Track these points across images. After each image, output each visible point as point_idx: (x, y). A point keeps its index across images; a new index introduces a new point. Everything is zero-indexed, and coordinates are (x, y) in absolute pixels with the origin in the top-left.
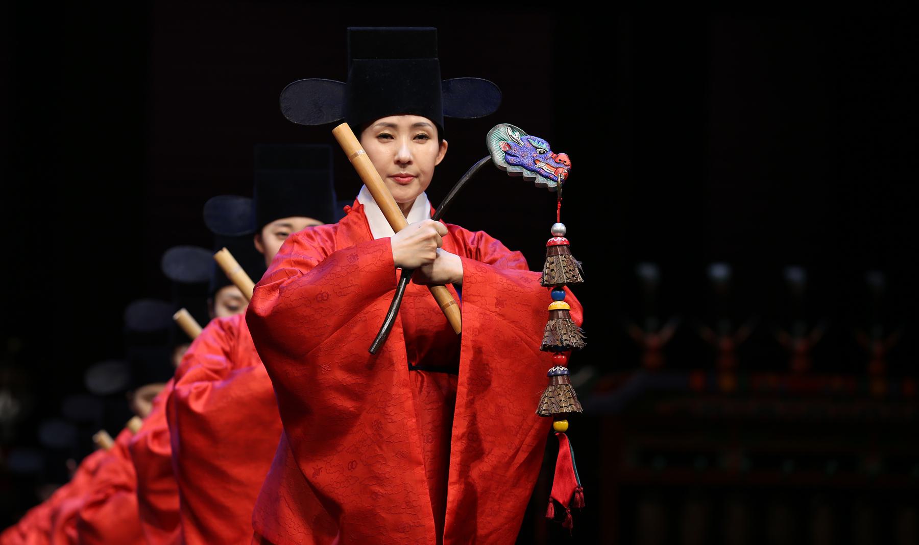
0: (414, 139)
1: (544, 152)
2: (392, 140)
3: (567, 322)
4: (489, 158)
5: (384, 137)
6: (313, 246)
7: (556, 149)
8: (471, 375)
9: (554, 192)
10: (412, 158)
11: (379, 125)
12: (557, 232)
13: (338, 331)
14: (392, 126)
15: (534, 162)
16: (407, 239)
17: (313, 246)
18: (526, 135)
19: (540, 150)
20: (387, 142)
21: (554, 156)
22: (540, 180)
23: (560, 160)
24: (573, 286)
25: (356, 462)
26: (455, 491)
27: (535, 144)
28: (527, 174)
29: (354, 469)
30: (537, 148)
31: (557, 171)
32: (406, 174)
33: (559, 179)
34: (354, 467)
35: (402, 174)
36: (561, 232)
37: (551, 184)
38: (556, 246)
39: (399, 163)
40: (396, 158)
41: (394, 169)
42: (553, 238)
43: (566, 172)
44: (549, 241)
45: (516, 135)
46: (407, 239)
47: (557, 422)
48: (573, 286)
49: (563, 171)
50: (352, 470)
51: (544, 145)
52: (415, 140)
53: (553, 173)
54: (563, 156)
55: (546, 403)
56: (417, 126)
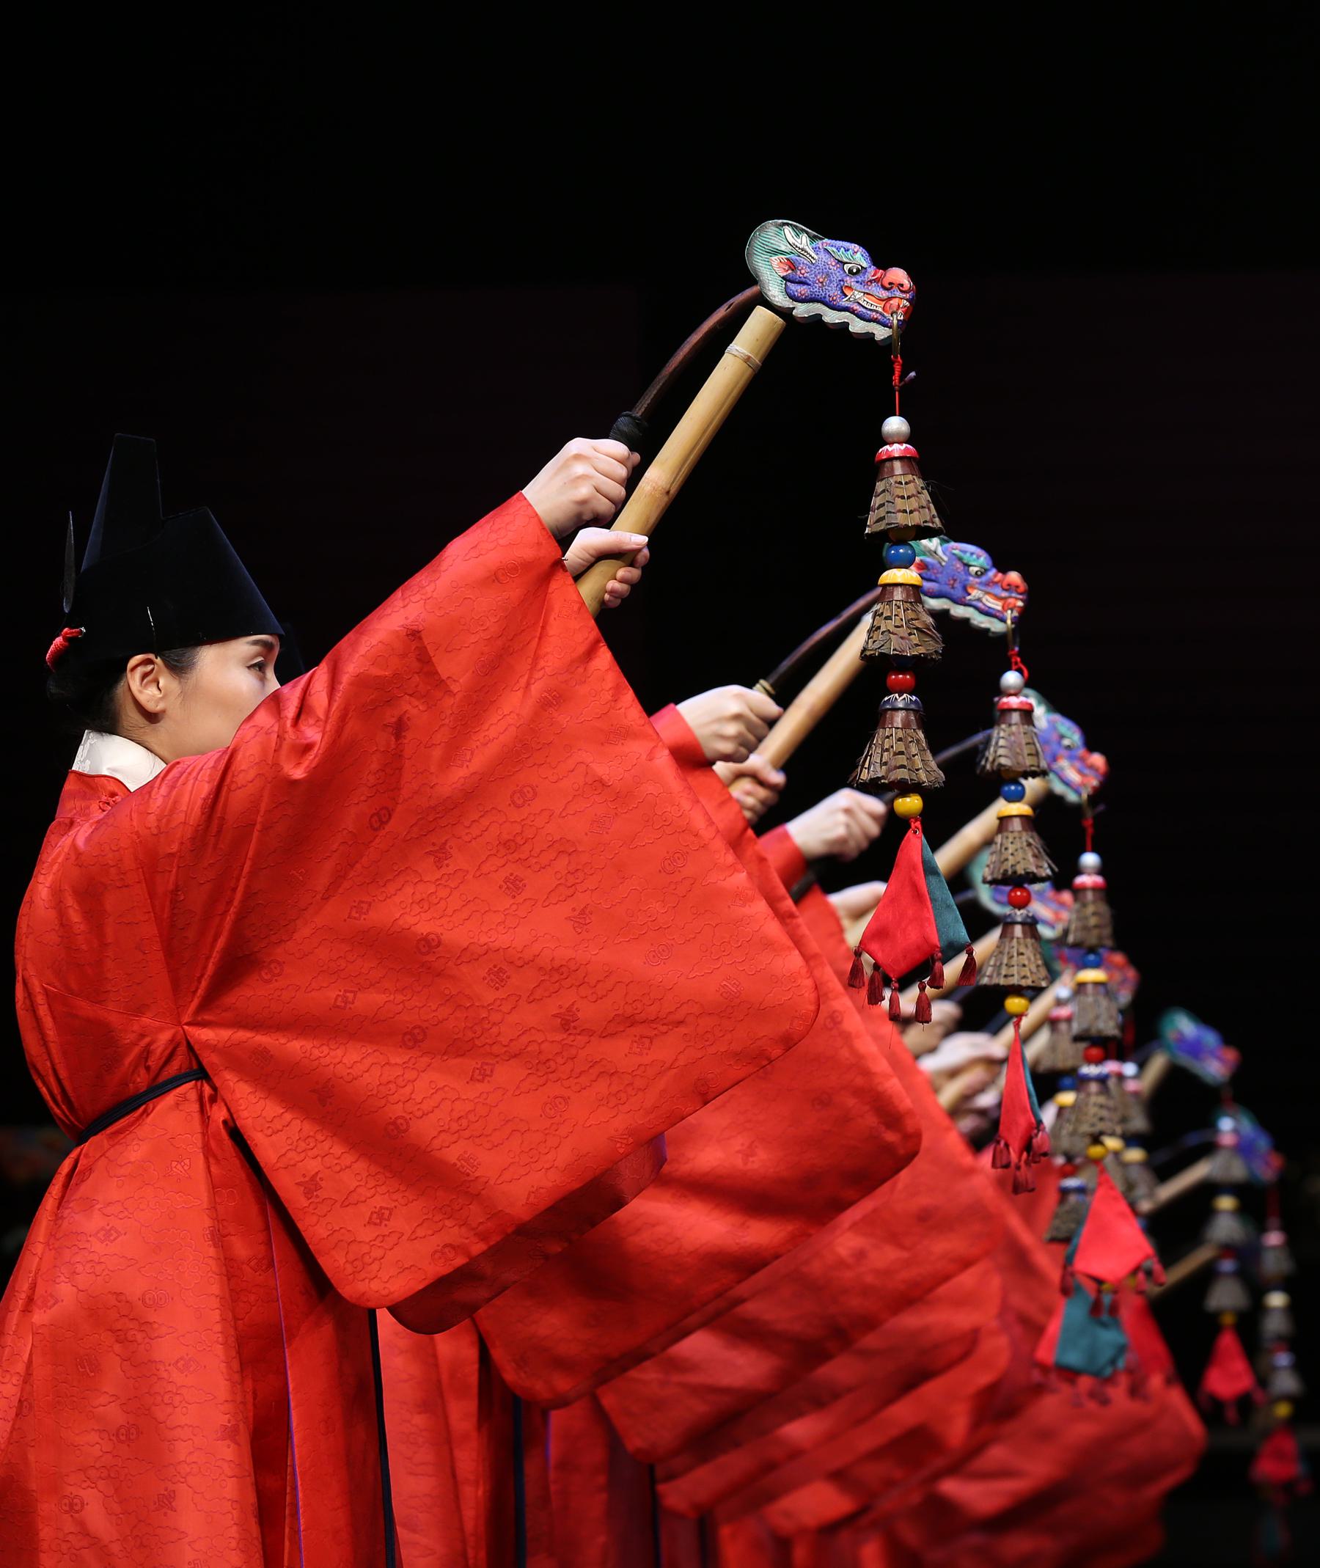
1: (858, 271)
4: (754, 289)
7: (882, 261)
8: (1007, 770)
9: (887, 345)
12: (891, 435)
13: (286, 1346)
15: (843, 292)
16: (33, 1287)
18: (821, 239)
19: (850, 265)
21: (879, 275)
22: (857, 326)
23: (890, 284)
27: (842, 255)
28: (831, 317)
31: (888, 305)
33: (895, 322)
36: (898, 434)
37: (881, 333)
38: (892, 459)
42: (887, 447)
43: (908, 304)
44: (880, 450)
45: (803, 241)
46: (33, 1287)
47: (900, 800)
49: (901, 302)
51: (857, 256)
53: (880, 310)
54: (899, 275)
55: (374, 753)
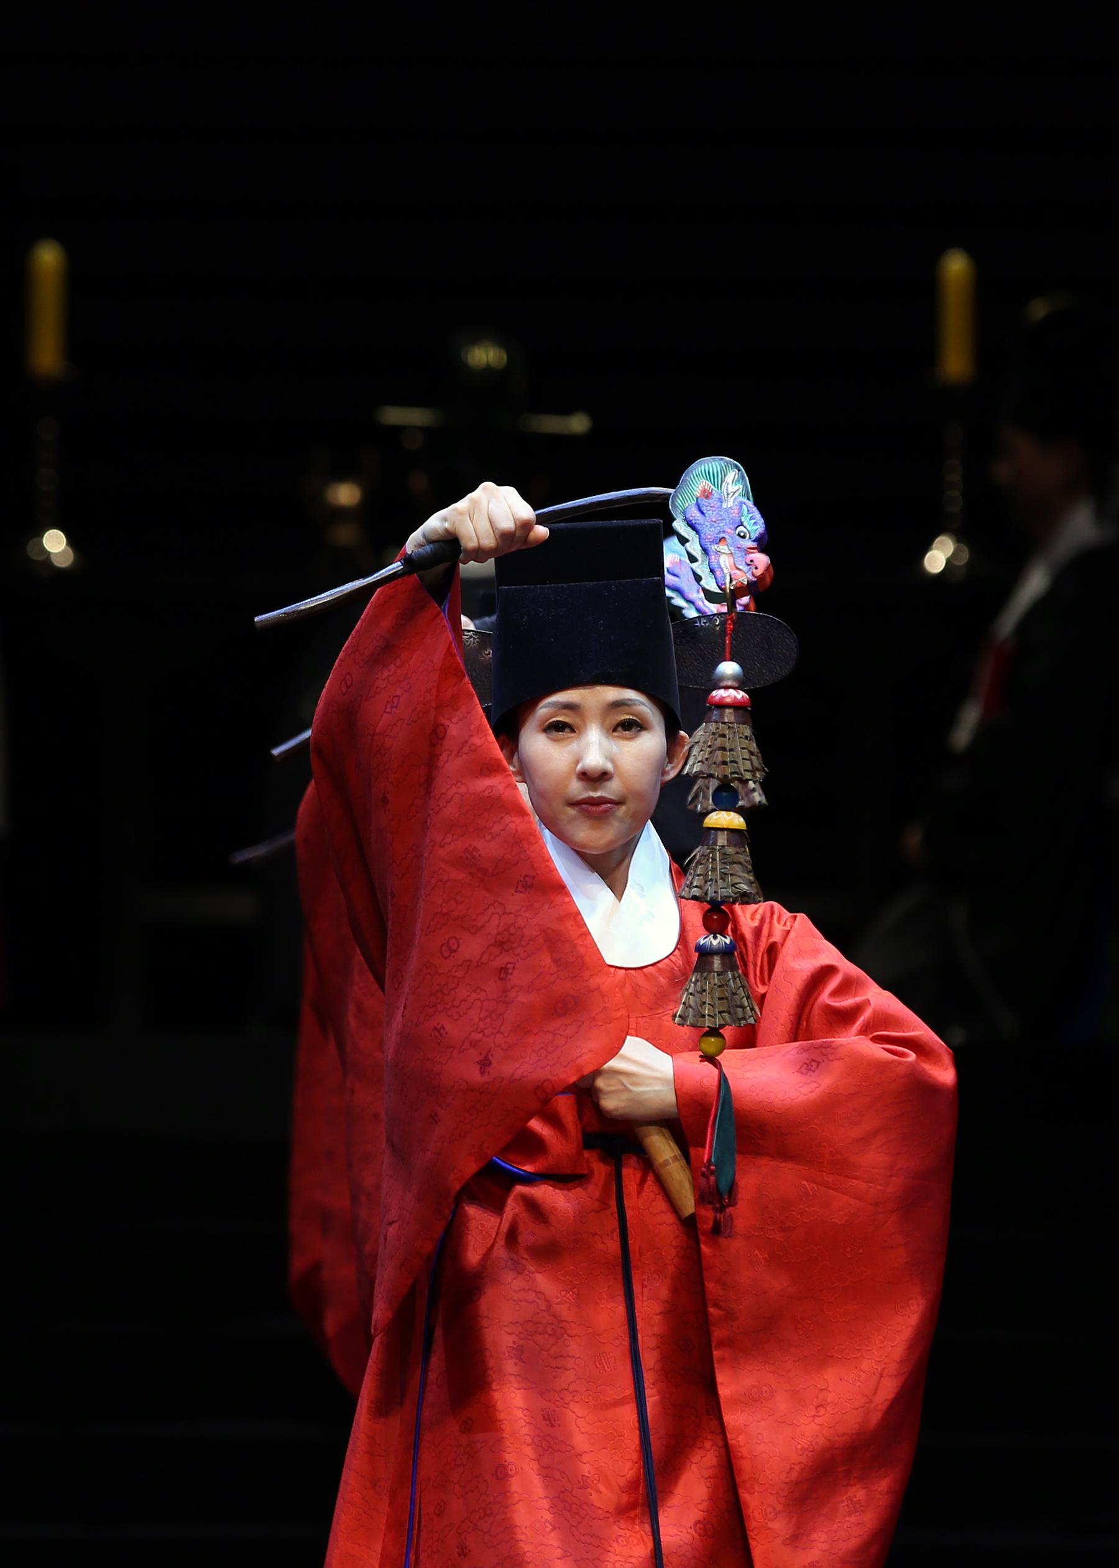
0: (615, 730)
2: (573, 735)
3: (711, 507)
5: (556, 728)
6: (493, 1246)
7: (763, 544)
10: (609, 767)
11: (545, 709)
14: (570, 707)
17: (493, 1246)
20: (563, 739)
24: (760, 782)
25: (454, 937)
26: (675, 1247)
29: (455, 951)
30: (742, 525)
32: (599, 797)
34: (455, 947)
35: (592, 798)
39: (585, 776)
40: (579, 767)
41: (577, 789)
48: (760, 782)
50: (454, 954)
52: (615, 734)
56: (617, 705)
